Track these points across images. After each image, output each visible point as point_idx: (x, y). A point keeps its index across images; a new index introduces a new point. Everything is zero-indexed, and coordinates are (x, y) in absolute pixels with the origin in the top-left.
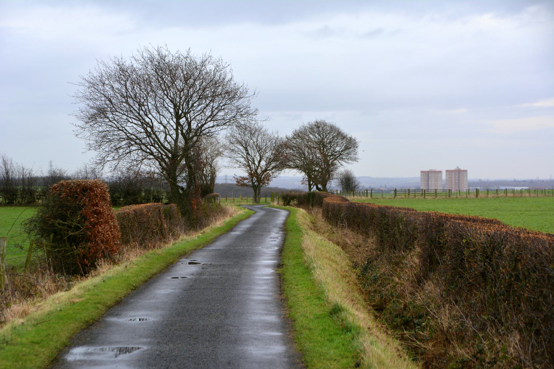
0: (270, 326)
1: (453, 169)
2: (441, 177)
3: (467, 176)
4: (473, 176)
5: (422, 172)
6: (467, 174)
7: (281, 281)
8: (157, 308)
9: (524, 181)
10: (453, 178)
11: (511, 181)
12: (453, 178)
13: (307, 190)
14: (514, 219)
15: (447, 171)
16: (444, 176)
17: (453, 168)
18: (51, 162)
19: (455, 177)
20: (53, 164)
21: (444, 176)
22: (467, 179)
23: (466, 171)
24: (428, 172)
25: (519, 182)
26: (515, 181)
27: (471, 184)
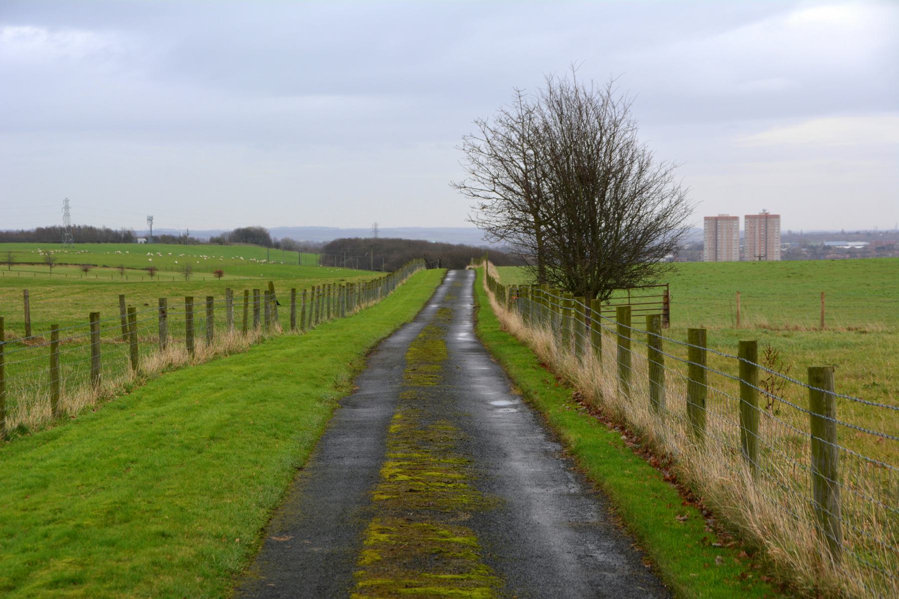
0: (484, 374)
1: (757, 213)
2: (738, 226)
3: (779, 224)
4: (794, 222)
5: (706, 219)
6: (779, 221)
7: (474, 290)
8: (388, 349)
9: (858, 233)
10: (757, 229)
11: (837, 234)
12: (757, 229)
13: (148, 229)
14: (501, 251)
15: (747, 217)
16: (742, 226)
17: (756, 212)
18: (67, 201)
19: (760, 227)
20: (70, 204)
21: (742, 226)
22: (779, 229)
23: (777, 217)
24: (716, 219)
25: (850, 234)
26: (843, 233)
27: (790, 237)
